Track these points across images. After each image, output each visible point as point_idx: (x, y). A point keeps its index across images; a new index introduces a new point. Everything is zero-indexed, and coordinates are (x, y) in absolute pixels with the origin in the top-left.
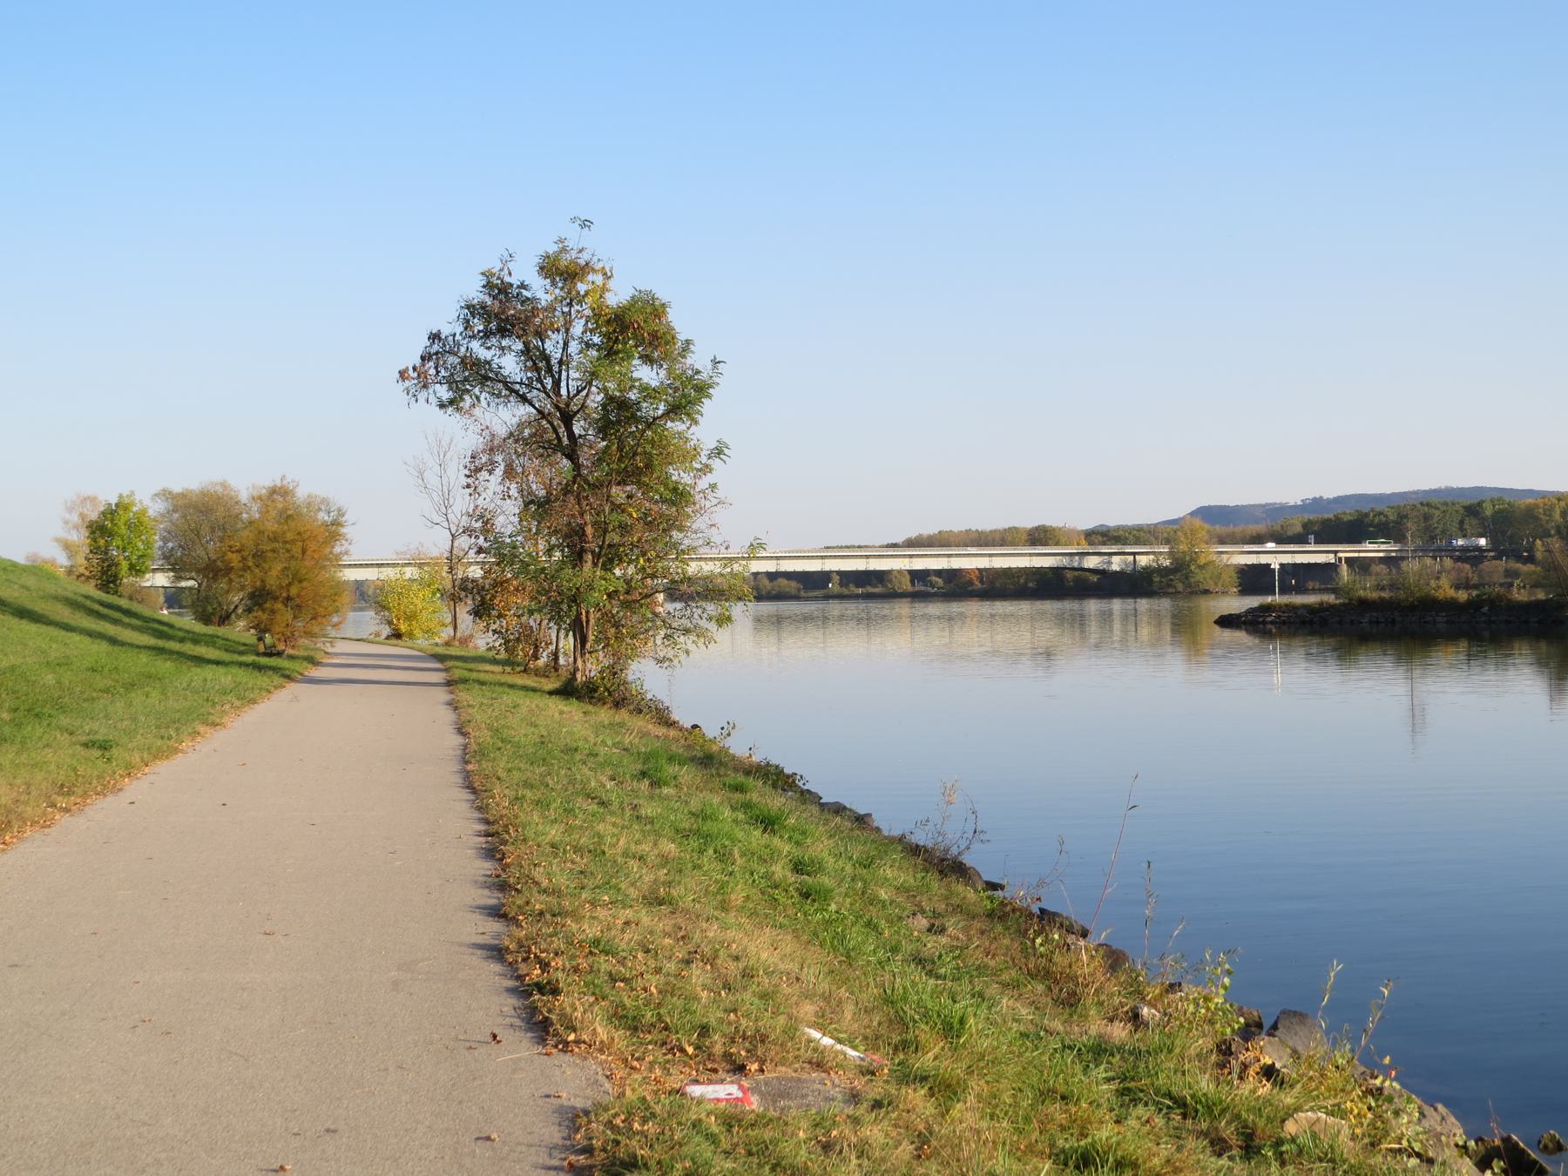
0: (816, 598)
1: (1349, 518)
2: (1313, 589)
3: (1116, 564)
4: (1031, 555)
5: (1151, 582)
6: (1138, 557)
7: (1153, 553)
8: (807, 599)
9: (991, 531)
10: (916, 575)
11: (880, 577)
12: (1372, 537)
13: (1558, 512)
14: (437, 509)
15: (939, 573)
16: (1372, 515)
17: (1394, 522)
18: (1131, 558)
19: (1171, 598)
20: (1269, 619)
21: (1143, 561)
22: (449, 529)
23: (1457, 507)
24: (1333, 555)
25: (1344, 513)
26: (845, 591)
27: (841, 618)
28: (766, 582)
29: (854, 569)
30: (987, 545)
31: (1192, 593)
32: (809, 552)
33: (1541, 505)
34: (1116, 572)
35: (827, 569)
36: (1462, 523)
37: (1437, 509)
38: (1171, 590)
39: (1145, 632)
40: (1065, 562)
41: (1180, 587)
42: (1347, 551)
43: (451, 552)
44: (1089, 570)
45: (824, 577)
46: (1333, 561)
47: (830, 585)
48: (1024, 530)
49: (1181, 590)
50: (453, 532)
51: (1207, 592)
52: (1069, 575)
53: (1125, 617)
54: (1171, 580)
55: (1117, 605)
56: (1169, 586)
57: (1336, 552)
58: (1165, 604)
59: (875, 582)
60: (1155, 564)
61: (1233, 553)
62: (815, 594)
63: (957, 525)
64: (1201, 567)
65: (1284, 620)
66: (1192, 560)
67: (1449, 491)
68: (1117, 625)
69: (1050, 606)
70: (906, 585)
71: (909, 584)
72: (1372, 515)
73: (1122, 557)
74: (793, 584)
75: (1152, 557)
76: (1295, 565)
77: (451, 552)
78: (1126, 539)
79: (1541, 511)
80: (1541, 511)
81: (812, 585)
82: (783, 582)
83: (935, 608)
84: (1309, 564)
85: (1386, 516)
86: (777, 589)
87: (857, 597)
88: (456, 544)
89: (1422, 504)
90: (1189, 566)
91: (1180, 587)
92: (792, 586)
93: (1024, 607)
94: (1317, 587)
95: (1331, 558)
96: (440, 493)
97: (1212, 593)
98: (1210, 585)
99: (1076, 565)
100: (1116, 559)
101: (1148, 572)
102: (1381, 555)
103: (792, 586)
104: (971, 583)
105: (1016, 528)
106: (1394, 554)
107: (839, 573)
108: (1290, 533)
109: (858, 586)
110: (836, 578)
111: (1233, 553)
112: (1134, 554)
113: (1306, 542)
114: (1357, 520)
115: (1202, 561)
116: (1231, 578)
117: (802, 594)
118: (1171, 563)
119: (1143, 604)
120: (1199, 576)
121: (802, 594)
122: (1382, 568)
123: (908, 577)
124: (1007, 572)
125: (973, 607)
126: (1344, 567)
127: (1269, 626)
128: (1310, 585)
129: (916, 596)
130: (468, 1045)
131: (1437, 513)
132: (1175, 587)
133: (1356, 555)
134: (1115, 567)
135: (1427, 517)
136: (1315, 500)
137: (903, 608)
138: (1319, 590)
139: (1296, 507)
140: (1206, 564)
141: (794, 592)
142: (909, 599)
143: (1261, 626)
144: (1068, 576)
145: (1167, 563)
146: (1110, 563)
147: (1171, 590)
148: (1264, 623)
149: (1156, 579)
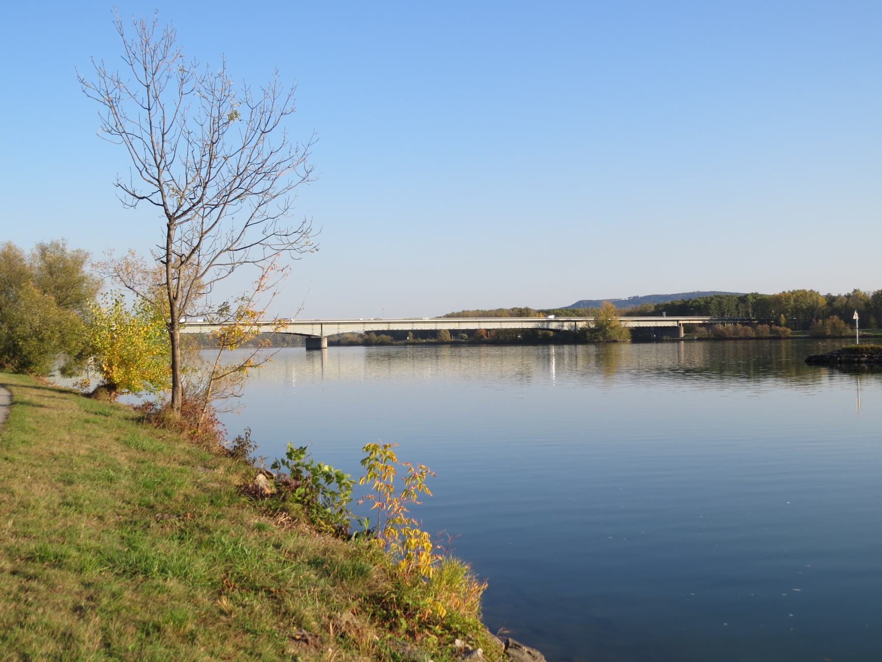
0: (401, 345)
1: (679, 303)
2: (666, 340)
3: (566, 327)
4: (522, 322)
5: (585, 336)
6: (577, 323)
7: (586, 321)
8: (396, 345)
9: (489, 311)
10: (454, 332)
11: (434, 333)
12: (692, 314)
13: (792, 300)
14: (141, 167)
15: (464, 331)
16: (691, 302)
17: (703, 305)
18: (574, 323)
19: (595, 345)
20: (863, 359)
21: (580, 325)
22: (164, 205)
23: (735, 298)
24: (676, 322)
25: (677, 301)
26: (416, 341)
27: (487, 355)
28: (374, 336)
29: (429, 329)
30: (491, 316)
31: (607, 342)
32: (409, 319)
33: (784, 296)
34: (566, 331)
35: (438, 328)
36: (737, 306)
37: (725, 299)
38: (596, 340)
39: (581, 362)
40: (540, 325)
41: (601, 339)
42: (684, 320)
43: (168, 249)
44: (552, 330)
45: (405, 333)
46: (676, 325)
47: (408, 338)
48: (507, 310)
49: (602, 340)
50: (171, 212)
51: (615, 341)
52: (540, 333)
53: (570, 354)
54: (596, 335)
55: (566, 349)
56: (595, 338)
57: (678, 321)
58: (592, 349)
59: (430, 336)
60: (587, 327)
61: (628, 321)
62: (401, 342)
63: (472, 308)
64: (612, 328)
65: (877, 360)
66: (607, 324)
67: (699, 293)
68: (566, 361)
69: (531, 349)
70: (448, 337)
71: (450, 337)
72: (691, 302)
73: (570, 323)
74: (389, 337)
75: (585, 323)
76: (657, 328)
77: (168, 249)
78: (561, 314)
79: (783, 299)
80: (783, 299)
81: (398, 338)
82: (383, 336)
83: (464, 351)
84: (664, 327)
85: (699, 302)
86: (380, 340)
87: (422, 344)
88: (176, 234)
89: (715, 296)
90: (605, 327)
91: (601, 339)
92: (388, 338)
93: (518, 350)
94: (668, 339)
95: (675, 324)
96: (147, 139)
97: (618, 342)
98: (617, 338)
99: (545, 327)
100: (566, 324)
101: (583, 331)
102: (701, 322)
103: (388, 338)
104: (482, 337)
105: (502, 309)
106: (707, 322)
107: (412, 331)
108: (648, 311)
109: (422, 339)
110: (411, 334)
111: (628, 321)
112: (575, 321)
113: (661, 315)
114: (683, 304)
115: (613, 325)
116: (626, 334)
117: (394, 342)
118: (595, 326)
119: (580, 349)
120: (611, 333)
121: (394, 342)
122: (703, 329)
123: (449, 334)
124: (506, 331)
125: (485, 350)
126: (682, 329)
127: (864, 365)
128: (665, 338)
129: (455, 344)
130: (232, 257)
131: (725, 301)
132: (598, 339)
133: (688, 322)
134: (566, 328)
135: (720, 303)
136: (634, 297)
137: (446, 351)
138: (670, 340)
139: (625, 301)
140: (615, 327)
141: (389, 341)
142: (449, 345)
143: (856, 365)
144: (540, 333)
145: (592, 326)
146: (563, 326)
147: (596, 340)
148: (859, 362)
149: (588, 334)
